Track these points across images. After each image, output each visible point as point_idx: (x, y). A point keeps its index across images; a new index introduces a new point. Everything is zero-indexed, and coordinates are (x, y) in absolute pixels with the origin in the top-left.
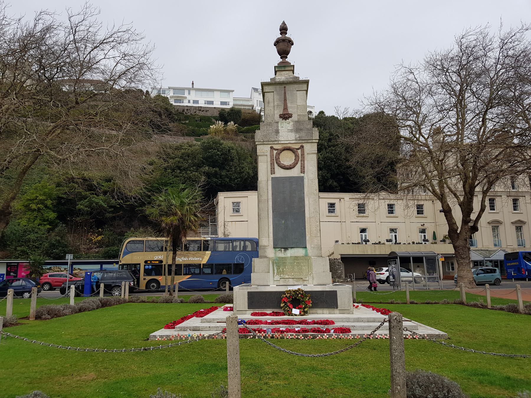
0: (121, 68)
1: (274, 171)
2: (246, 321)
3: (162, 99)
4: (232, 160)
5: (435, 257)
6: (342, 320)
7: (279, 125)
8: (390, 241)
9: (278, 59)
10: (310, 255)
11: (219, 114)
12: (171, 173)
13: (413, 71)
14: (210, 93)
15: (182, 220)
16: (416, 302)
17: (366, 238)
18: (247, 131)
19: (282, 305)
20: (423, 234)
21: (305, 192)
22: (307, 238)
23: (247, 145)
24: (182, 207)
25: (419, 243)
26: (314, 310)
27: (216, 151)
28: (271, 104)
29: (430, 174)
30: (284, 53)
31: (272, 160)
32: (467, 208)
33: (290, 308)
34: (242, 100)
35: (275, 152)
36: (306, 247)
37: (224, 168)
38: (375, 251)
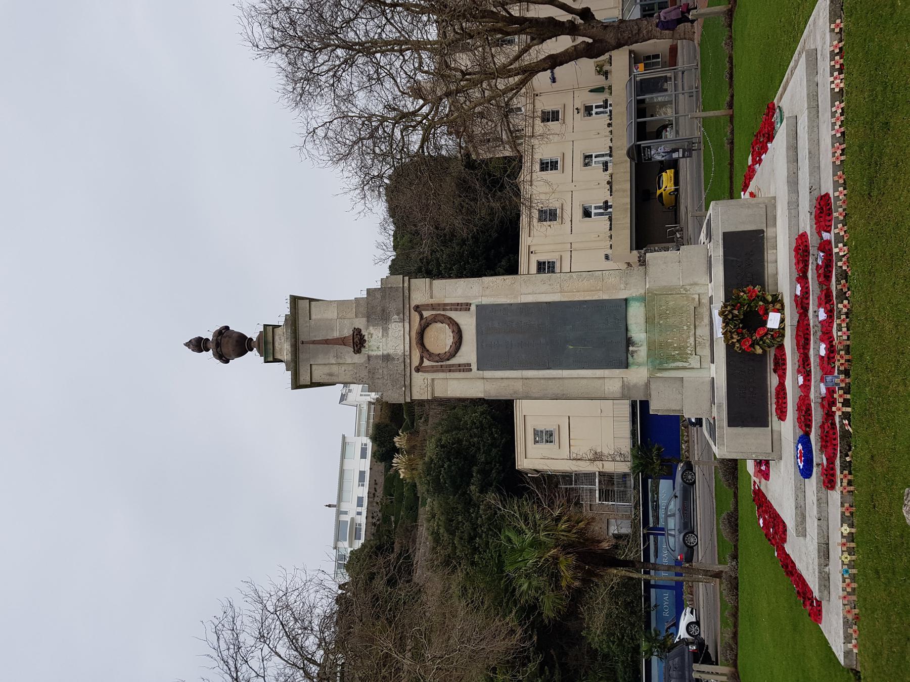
0: (283, 648)
1: (465, 365)
2: (800, 433)
3: (354, 563)
4: (459, 441)
5: (636, 82)
6: (794, 215)
7: (374, 353)
8: (605, 165)
9: (253, 356)
10: (643, 292)
11: (381, 461)
12: (480, 553)
13: (311, 130)
14: (346, 476)
15: (567, 548)
16: (728, 98)
17: (600, 208)
18: (412, 415)
19: (759, 351)
20: (594, 111)
21: (508, 302)
22: (606, 297)
23: (435, 415)
24: (540, 544)
25: (610, 115)
26: (769, 280)
27: (445, 473)
28: (335, 369)
29: (487, 93)
30: (242, 345)
31: (442, 369)
32: (550, 28)
33: (766, 334)
34: (359, 424)
35: (426, 363)
36: (626, 300)
37: (474, 456)
38: (624, 191)
